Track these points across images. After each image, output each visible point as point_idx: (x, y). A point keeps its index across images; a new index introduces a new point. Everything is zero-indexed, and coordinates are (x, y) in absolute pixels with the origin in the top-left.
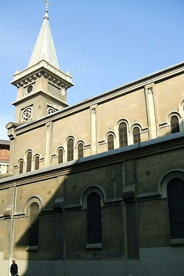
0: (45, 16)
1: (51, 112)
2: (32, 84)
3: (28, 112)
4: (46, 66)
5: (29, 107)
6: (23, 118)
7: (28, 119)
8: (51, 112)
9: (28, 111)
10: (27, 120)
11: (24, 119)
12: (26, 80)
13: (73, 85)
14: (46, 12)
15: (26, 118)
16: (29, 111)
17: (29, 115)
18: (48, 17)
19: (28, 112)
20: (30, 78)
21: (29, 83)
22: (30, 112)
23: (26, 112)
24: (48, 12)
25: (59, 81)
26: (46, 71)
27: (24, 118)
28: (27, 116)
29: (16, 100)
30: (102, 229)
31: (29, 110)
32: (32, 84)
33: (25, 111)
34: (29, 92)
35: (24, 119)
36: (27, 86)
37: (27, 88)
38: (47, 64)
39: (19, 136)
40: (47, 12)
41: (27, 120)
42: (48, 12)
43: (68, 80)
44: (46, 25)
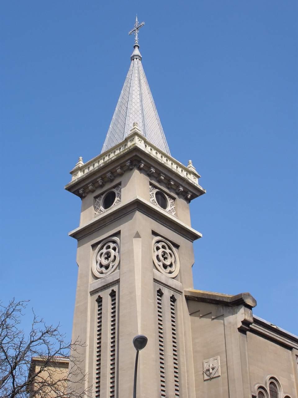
0: (133, 55)
4: (141, 145)
6: (98, 263)
7: (111, 266)
10: (107, 267)
11: (101, 266)
13: (202, 193)
14: (134, 47)
15: (105, 262)
16: (111, 247)
18: (140, 55)
19: (111, 250)
20: (81, 192)
21: (107, 187)
22: (114, 249)
23: (104, 250)
25: (154, 167)
26: (95, 177)
28: (107, 258)
29: (78, 226)
30: (197, 296)
31: (112, 245)
33: (102, 248)
34: (107, 205)
35: (101, 266)
36: (102, 194)
37: (103, 197)
38: (143, 142)
39: (100, 287)
41: (107, 267)
42: (138, 47)
44: (137, 67)
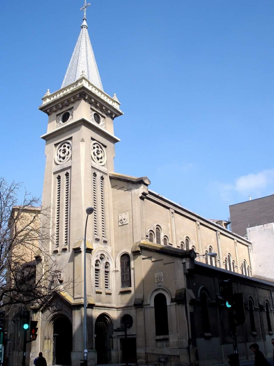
0: (82, 25)
1: (96, 147)
2: (69, 110)
3: (65, 148)
4: (86, 85)
5: (65, 141)
8: (96, 147)
9: (65, 146)
10: (64, 158)
11: (60, 157)
12: (73, 98)
13: (121, 114)
15: (62, 155)
17: (67, 153)
19: (66, 148)
22: (68, 147)
23: (62, 148)
24: (86, 20)
25: (94, 99)
26: (57, 103)
27: (60, 155)
31: (67, 145)
32: (69, 110)
33: (61, 146)
34: (65, 119)
37: (62, 115)
38: (88, 83)
40: (85, 20)
41: (64, 158)
42: (86, 20)
43: (116, 106)
